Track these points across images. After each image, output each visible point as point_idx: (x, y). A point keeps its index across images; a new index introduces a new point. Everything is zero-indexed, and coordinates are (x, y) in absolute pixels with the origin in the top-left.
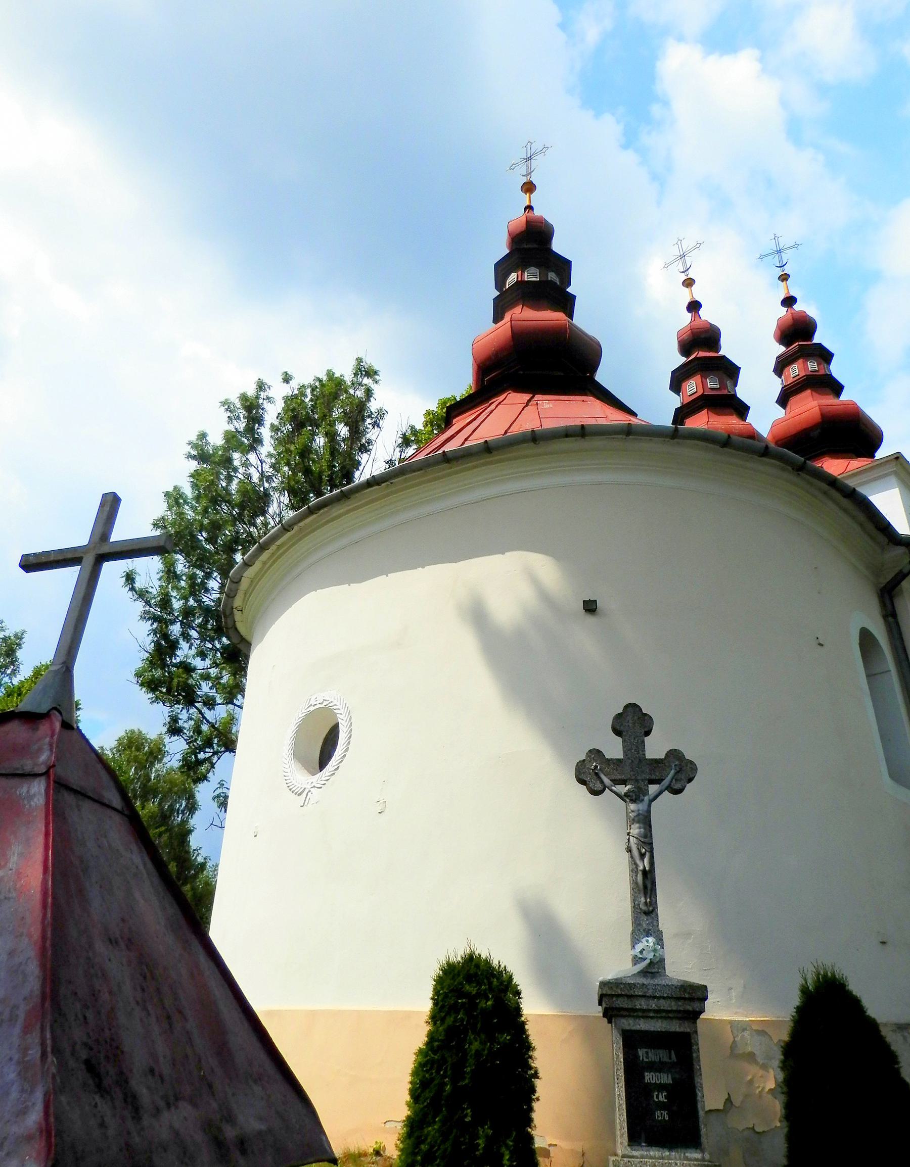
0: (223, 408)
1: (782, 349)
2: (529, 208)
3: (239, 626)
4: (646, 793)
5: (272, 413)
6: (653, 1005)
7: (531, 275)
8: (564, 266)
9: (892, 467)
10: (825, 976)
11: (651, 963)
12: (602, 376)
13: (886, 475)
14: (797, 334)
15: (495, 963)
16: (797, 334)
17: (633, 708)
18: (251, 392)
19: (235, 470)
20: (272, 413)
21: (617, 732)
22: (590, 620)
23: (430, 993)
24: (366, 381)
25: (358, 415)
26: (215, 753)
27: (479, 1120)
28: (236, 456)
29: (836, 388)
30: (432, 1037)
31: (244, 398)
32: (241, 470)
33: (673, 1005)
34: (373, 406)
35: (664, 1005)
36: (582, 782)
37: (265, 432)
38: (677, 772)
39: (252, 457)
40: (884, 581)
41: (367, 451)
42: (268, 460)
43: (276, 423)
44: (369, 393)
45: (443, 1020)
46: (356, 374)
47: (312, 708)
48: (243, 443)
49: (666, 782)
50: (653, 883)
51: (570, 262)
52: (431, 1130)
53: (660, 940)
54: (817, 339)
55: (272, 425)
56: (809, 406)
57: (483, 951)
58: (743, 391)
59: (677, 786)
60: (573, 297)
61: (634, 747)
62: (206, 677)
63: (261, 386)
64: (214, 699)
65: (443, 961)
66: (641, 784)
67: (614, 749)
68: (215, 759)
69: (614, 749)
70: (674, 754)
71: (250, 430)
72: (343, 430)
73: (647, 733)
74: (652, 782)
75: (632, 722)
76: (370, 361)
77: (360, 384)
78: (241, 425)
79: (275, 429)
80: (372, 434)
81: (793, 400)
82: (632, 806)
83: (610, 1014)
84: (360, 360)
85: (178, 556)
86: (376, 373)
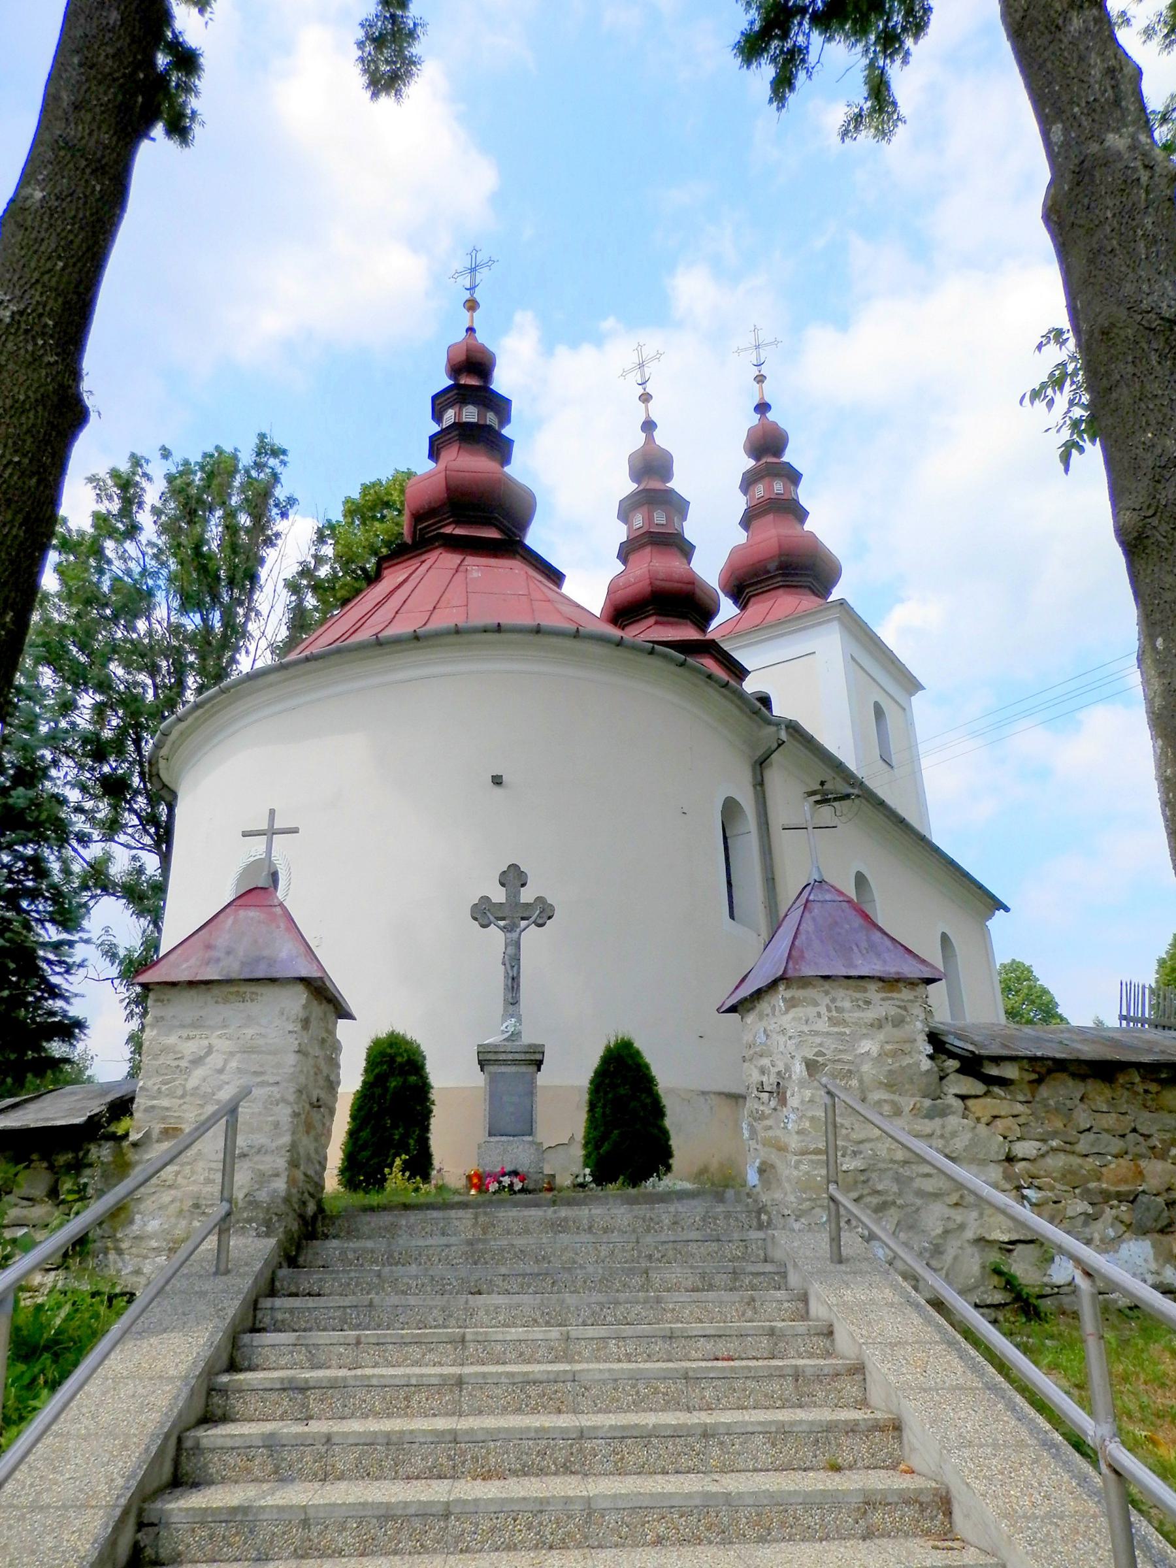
0: (90, 486)
1: (751, 463)
2: (471, 330)
3: (163, 774)
4: (518, 926)
5: (153, 493)
6: (510, 1057)
7: (470, 414)
8: (499, 405)
9: (836, 613)
10: (623, 1039)
11: (512, 1034)
12: (535, 538)
13: (829, 621)
14: (767, 446)
15: (408, 1037)
16: (767, 446)
17: (514, 867)
18: (124, 467)
19: (109, 562)
20: (153, 493)
21: (503, 885)
22: (498, 791)
23: (364, 1056)
24: (272, 462)
25: (262, 501)
26: (92, 897)
27: (395, 1126)
28: (109, 546)
29: (800, 514)
30: (364, 1082)
31: (115, 474)
32: (117, 563)
33: (523, 1057)
34: (280, 493)
35: (517, 1056)
36: (475, 919)
37: (145, 518)
38: (542, 913)
39: (129, 546)
40: (759, 753)
41: (273, 545)
42: (150, 551)
43: (158, 504)
44: (275, 477)
45: (373, 1071)
46: (258, 454)
47: (252, 859)
48: (118, 529)
49: (532, 919)
50: (518, 985)
51: (510, 401)
52: (364, 1134)
53: (519, 1020)
54: (787, 457)
55: (153, 507)
56: (772, 532)
57: (400, 1030)
58: (691, 531)
59: (540, 921)
60: (510, 442)
61: (513, 896)
62: (79, 809)
63: (136, 461)
64: (89, 835)
65: (374, 1037)
66: (516, 920)
67: (499, 895)
68: (91, 903)
69: (499, 895)
70: (540, 899)
71: (126, 511)
72: (244, 520)
73: (523, 885)
74: (523, 919)
75: (513, 877)
76: (278, 439)
77: (265, 465)
78: (115, 506)
79: (157, 512)
80: (280, 526)
81: (756, 524)
82: (508, 935)
83: (482, 1064)
84: (262, 436)
85: (46, 669)
86: (284, 452)
